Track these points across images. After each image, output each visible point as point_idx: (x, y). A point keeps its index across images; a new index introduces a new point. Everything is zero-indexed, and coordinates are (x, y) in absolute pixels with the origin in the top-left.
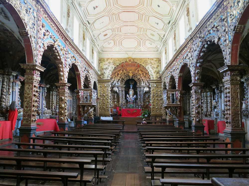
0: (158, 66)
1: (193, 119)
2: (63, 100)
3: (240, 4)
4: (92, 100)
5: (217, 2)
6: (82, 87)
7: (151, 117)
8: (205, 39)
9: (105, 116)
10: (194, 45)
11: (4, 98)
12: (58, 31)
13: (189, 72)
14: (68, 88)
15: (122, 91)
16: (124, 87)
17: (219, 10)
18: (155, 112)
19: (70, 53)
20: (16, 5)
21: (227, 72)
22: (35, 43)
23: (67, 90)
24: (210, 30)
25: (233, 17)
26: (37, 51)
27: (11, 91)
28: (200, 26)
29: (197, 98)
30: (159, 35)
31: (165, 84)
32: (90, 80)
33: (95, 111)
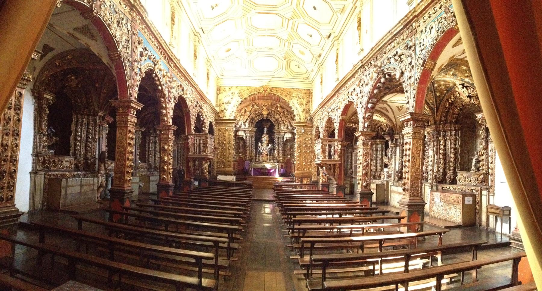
0: (308, 102)
1: (359, 183)
2: (166, 151)
3: (433, 31)
4: (207, 151)
5: (404, 20)
6: (193, 131)
7: (296, 178)
8: (382, 69)
9: (226, 174)
10: (366, 76)
11: (89, 147)
12: (159, 48)
13: (355, 113)
14: (173, 132)
15: (251, 138)
16: (255, 132)
17: (405, 31)
18: (301, 170)
19: (176, 81)
20: (105, 17)
21: (409, 122)
22: (129, 69)
23: (172, 137)
24: (391, 58)
25: (423, 47)
26: (133, 81)
27: (97, 137)
28: (376, 48)
29: (366, 153)
30: (313, 54)
31: (318, 130)
32: (203, 121)
33: (211, 167)
